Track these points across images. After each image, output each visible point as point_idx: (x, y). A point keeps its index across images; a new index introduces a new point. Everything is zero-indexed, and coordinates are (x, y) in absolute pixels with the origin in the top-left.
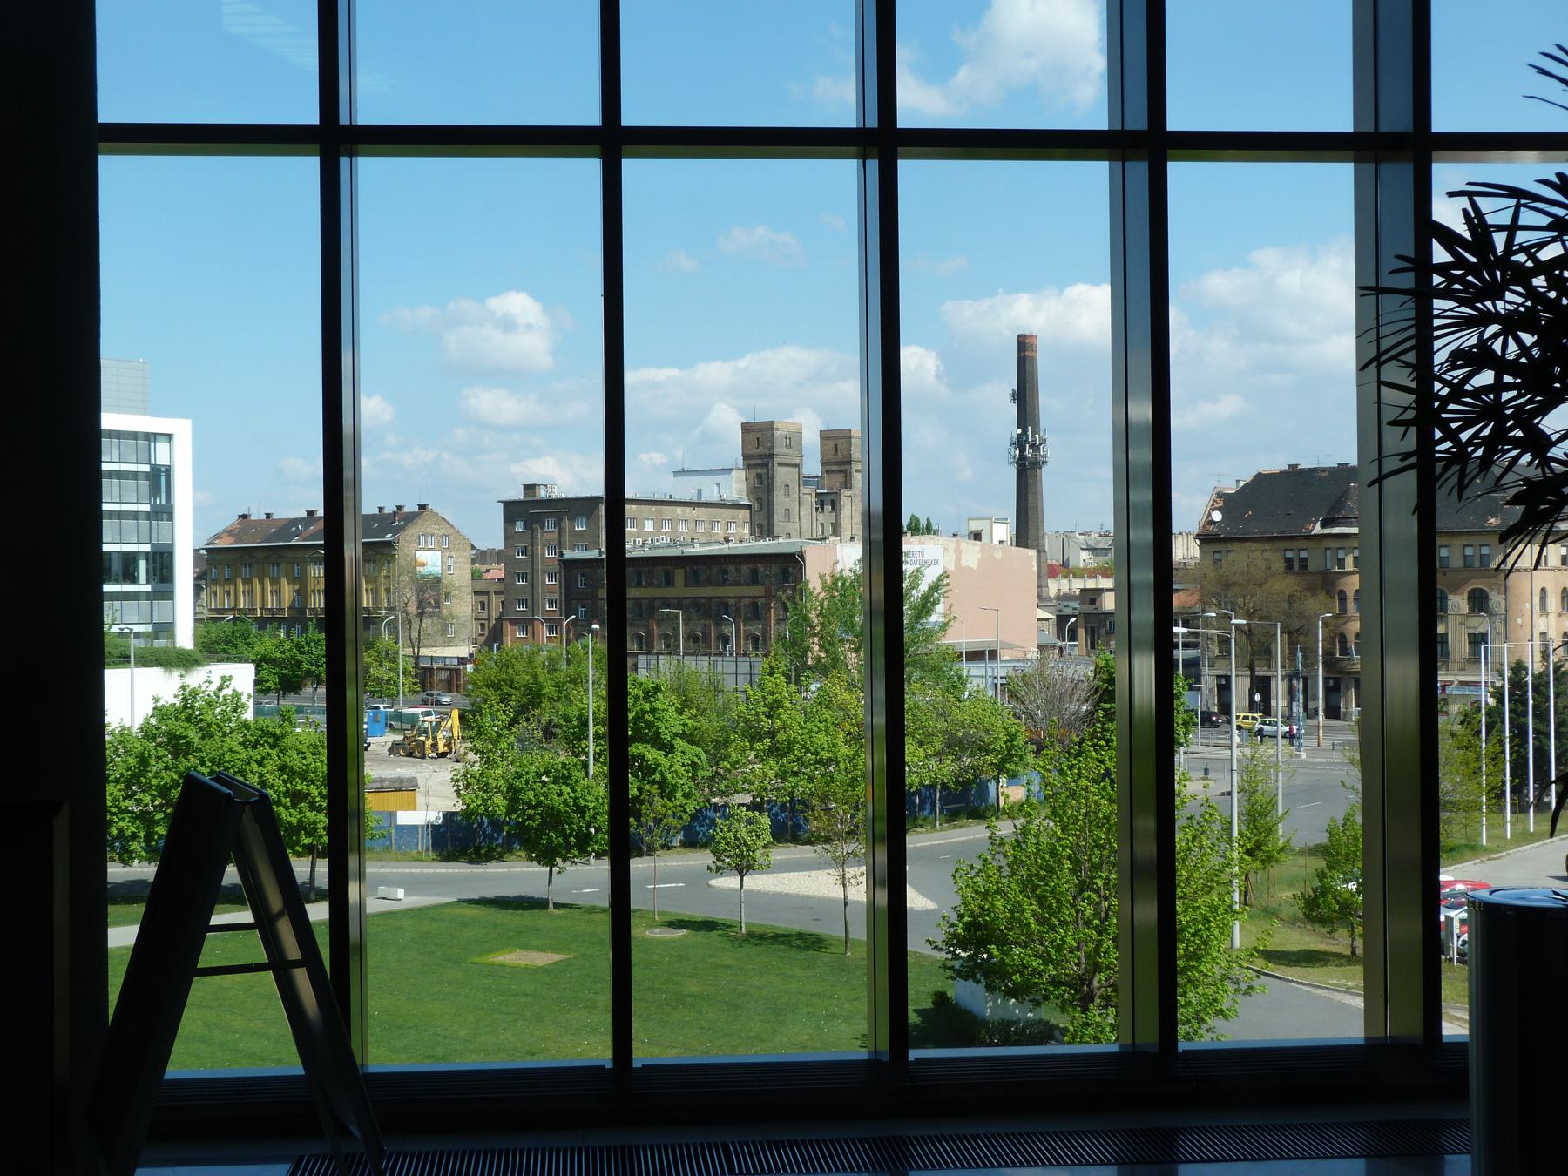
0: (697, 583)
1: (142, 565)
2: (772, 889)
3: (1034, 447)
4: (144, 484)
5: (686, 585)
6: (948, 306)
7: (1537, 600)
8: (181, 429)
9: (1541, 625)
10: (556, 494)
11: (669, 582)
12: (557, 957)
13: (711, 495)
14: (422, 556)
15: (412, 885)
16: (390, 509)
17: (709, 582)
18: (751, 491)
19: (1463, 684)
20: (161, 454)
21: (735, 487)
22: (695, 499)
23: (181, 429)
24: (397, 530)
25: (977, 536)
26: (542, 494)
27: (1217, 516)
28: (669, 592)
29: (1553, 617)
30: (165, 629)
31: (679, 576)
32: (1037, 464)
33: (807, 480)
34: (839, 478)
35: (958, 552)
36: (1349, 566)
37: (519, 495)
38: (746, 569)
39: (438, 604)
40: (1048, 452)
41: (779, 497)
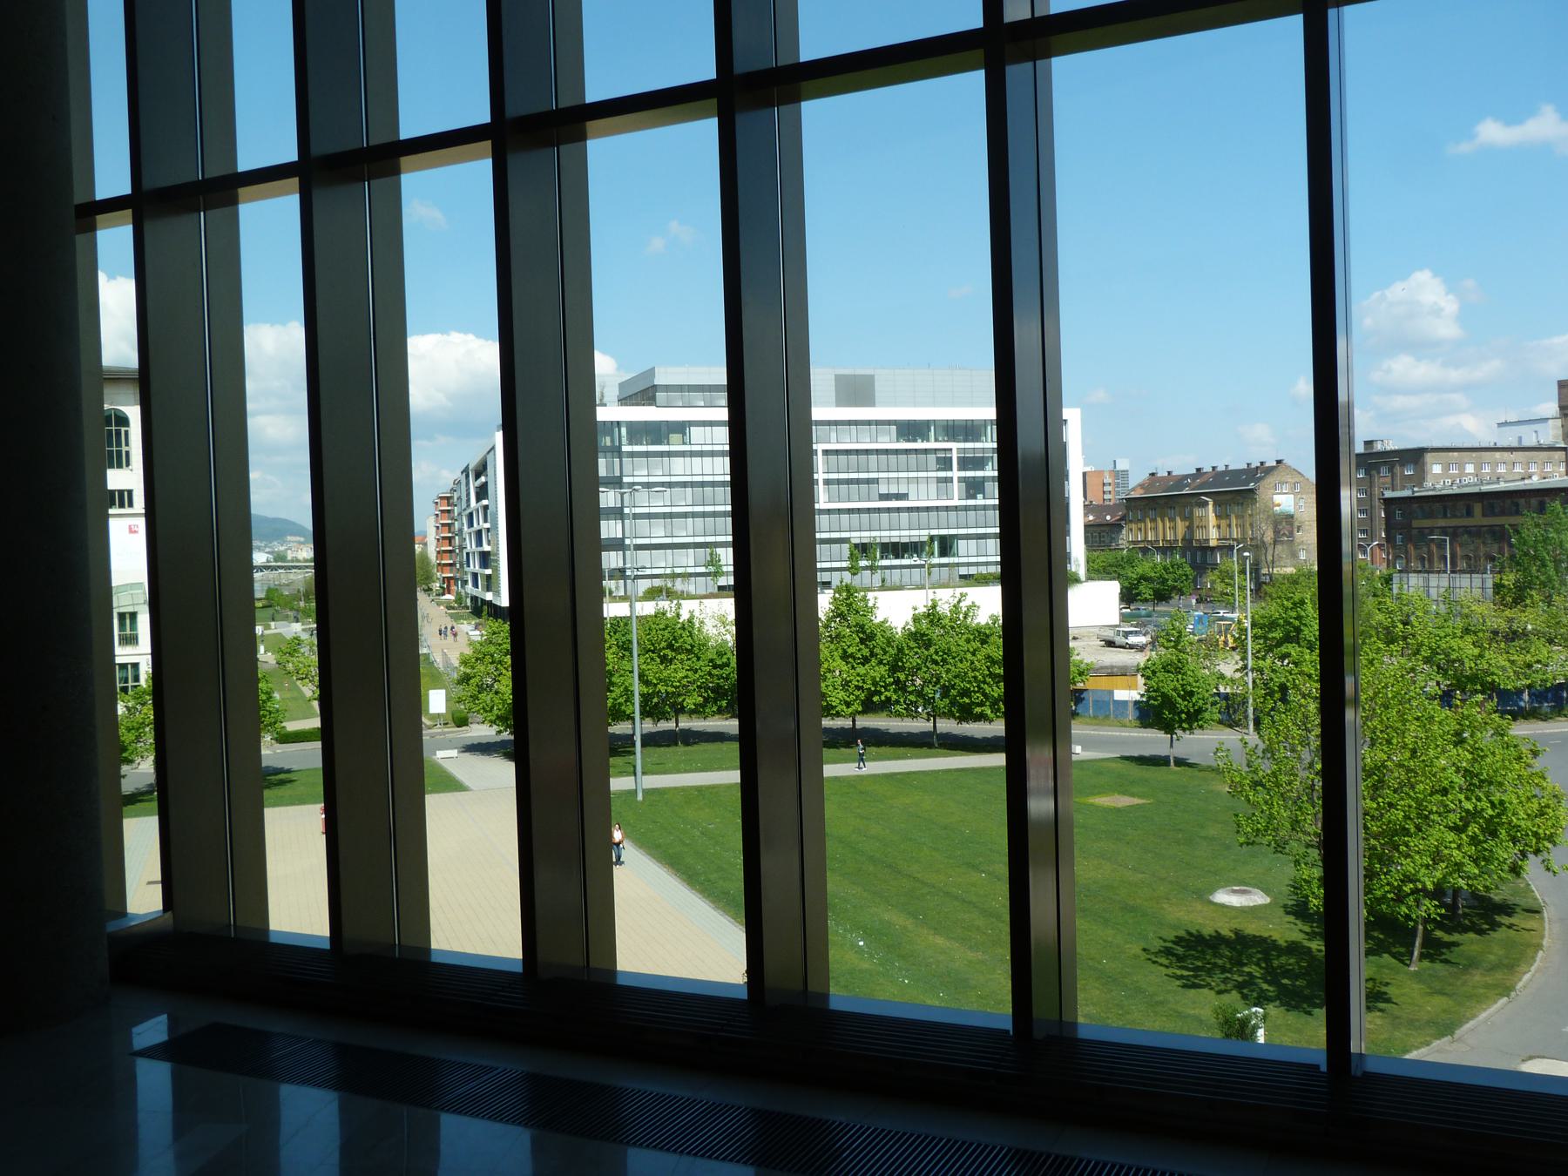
0: (1494, 514)
2: (724, 773)
5: (1484, 515)
10: (1391, 446)
12: (1137, 801)
13: (1530, 441)
14: (1277, 499)
16: (1255, 464)
17: (1503, 513)
22: (1515, 444)
26: (1379, 447)
38: (1534, 502)
39: (1291, 534)
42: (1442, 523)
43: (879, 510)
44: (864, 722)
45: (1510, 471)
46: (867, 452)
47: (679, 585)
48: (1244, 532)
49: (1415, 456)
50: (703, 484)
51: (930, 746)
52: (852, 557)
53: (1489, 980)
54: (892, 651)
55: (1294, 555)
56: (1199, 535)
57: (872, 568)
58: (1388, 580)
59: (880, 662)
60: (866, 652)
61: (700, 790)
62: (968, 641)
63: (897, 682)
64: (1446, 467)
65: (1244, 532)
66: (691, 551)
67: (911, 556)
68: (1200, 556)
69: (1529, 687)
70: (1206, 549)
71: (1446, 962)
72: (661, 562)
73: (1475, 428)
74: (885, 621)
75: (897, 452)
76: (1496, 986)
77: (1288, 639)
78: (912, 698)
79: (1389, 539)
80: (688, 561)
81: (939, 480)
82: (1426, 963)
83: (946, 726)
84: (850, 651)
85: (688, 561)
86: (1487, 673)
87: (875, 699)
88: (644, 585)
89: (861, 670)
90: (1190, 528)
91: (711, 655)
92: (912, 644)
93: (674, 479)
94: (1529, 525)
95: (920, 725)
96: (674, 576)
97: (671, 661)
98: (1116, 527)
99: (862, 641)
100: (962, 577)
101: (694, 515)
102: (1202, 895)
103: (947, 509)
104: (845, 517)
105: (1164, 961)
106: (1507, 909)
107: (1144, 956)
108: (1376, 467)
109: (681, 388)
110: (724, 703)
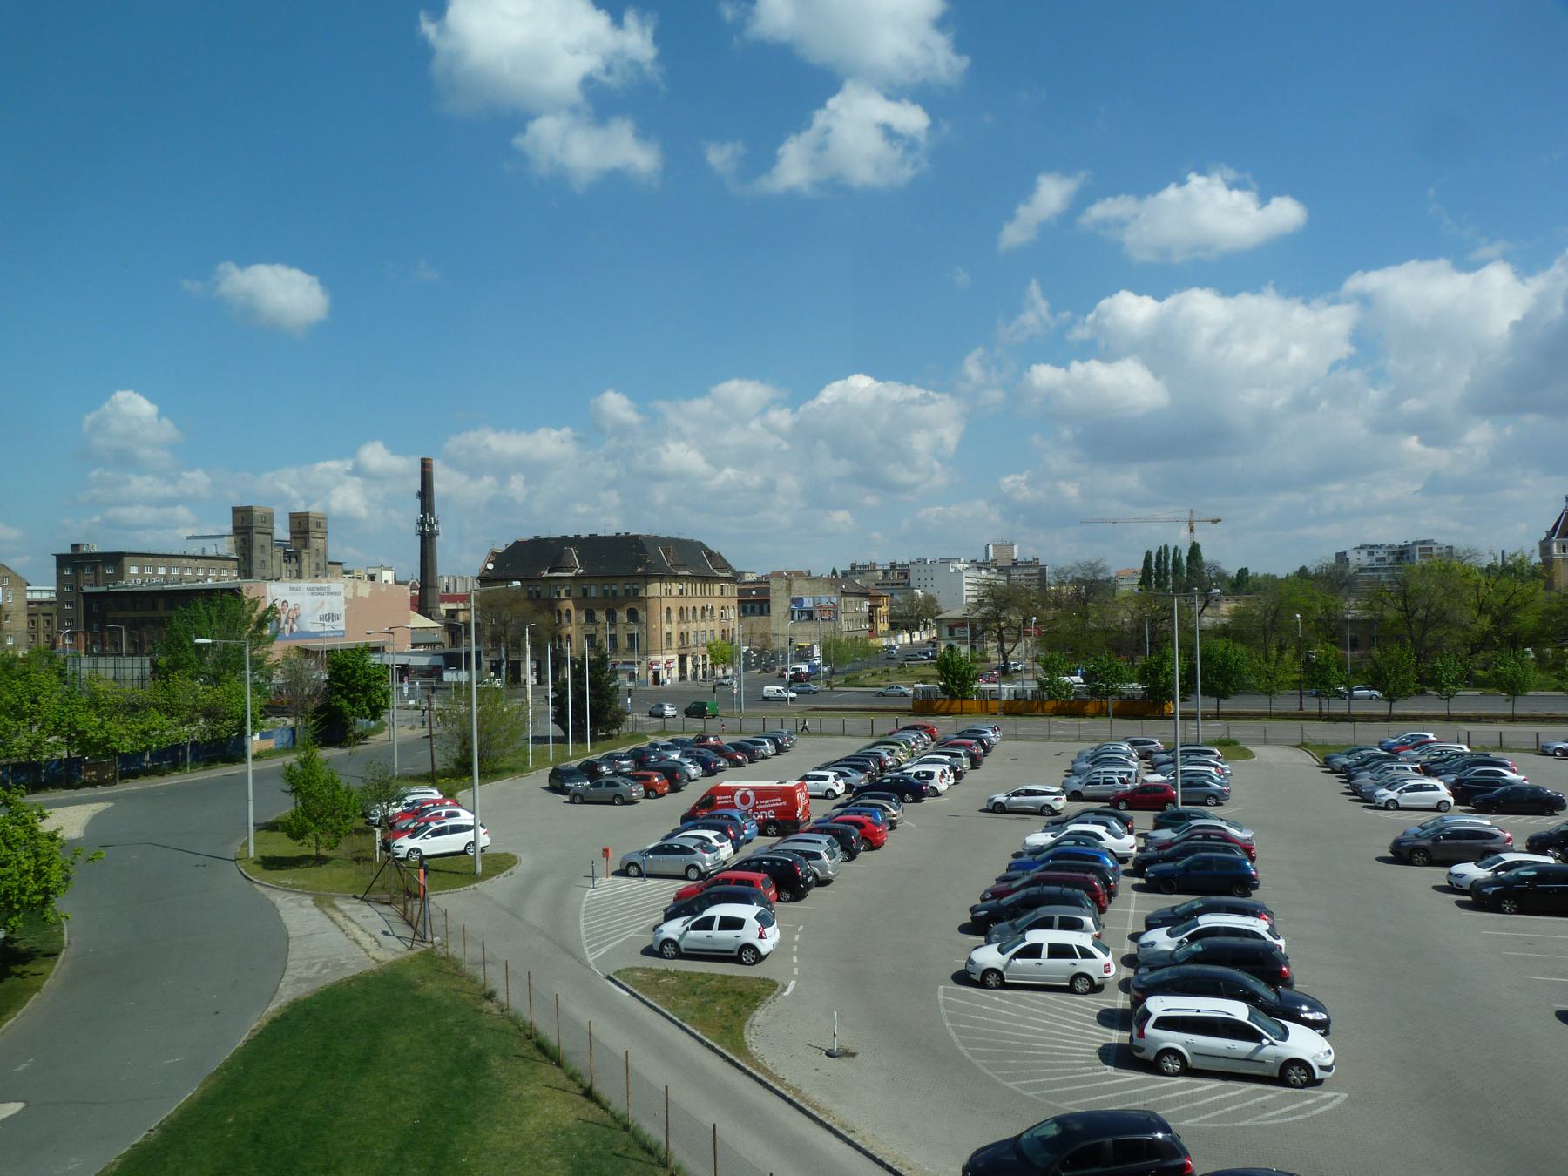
9: (667, 628)
10: (96, 549)
11: (154, 607)
13: (211, 551)
19: (625, 663)
21: (227, 547)
25: (372, 578)
27: (490, 566)
28: (151, 614)
29: (674, 624)
31: (161, 603)
32: (433, 535)
33: (281, 544)
34: (300, 543)
35: (355, 587)
36: (563, 595)
37: (67, 550)
40: (439, 528)
41: (257, 553)
42: (131, 614)
45: (194, 574)
64: (142, 570)
69: (148, 748)
73: (175, 540)
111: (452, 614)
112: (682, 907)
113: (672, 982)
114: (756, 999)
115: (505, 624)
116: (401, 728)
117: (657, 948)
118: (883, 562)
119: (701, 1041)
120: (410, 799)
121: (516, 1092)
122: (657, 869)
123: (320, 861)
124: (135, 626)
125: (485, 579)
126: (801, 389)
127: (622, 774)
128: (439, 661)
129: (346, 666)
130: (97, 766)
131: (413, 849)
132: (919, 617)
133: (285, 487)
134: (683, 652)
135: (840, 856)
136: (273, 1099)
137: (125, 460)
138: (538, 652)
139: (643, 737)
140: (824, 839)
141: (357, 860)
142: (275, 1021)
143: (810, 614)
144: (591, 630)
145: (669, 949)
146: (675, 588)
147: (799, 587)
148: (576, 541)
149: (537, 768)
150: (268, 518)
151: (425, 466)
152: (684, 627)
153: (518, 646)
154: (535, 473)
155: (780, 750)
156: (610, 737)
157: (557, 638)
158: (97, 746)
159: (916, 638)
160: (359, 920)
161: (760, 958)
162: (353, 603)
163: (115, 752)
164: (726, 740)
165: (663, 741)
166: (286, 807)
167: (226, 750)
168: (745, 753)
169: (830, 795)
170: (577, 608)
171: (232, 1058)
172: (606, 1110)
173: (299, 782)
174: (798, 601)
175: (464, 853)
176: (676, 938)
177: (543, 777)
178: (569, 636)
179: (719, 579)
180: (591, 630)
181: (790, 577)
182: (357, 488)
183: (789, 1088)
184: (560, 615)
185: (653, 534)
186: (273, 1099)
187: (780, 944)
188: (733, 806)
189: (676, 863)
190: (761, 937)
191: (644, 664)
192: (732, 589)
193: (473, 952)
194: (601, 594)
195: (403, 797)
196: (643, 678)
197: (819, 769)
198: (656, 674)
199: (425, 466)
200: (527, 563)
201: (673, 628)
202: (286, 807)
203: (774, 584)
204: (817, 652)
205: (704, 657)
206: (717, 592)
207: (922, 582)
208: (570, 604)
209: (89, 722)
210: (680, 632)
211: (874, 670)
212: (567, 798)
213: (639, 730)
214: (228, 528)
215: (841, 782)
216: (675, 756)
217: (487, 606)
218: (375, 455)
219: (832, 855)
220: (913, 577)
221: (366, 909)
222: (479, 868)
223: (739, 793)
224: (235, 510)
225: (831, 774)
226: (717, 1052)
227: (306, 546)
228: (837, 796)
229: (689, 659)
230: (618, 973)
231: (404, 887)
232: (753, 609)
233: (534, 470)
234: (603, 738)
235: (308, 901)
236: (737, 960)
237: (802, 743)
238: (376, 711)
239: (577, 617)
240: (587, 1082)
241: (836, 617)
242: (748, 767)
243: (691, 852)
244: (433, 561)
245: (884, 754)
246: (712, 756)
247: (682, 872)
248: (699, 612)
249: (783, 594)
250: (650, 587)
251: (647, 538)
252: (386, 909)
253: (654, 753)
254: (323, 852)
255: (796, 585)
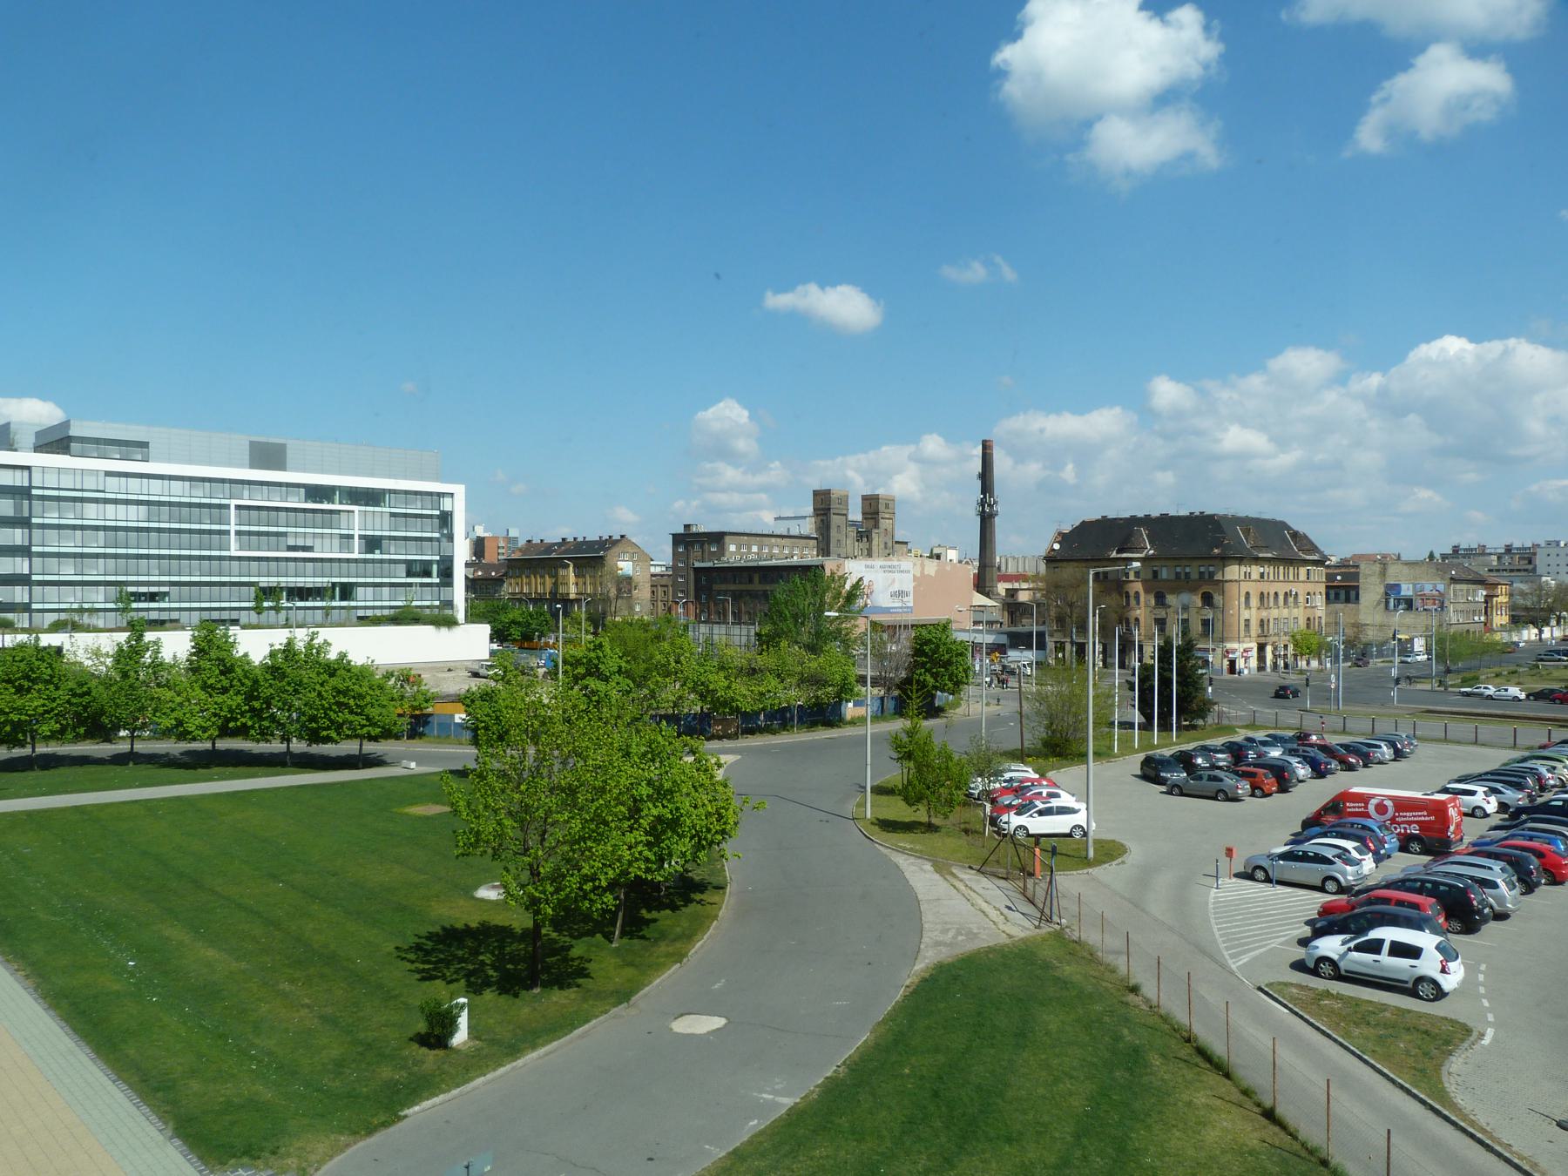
1: (435, 567)
3: (990, 506)
4: (436, 521)
6: (701, 415)
7: (1243, 599)
8: (459, 490)
9: (1245, 614)
10: (702, 530)
14: (620, 564)
15: (420, 760)
18: (818, 529)
20: (447, 505)
21: (808, 527)
23: (459, 490)
24: (606, 550)
26: (694, 530)
27: (1057, 546)
29: (1254, 610)
30: (449, 604)
31: (756, 578)
32: (992, 516)
33: (854, 524)
34: (872, 522)
35: (923, 565)
37: (681, 530)
40: (998, 508)
41: (833, 533)
42: (733, 587)
43: (287, 559)
44: (223, 744)
46: (277, 509)
47: (86, 619)
48: (595, 588)
49: (718, 538)
50: (116, 529)
51: (283, 764)
52: (257, 599)
53: (671, 949)
54: (248, 683)
55: (631, 608)
56: (562, 590)
57: (277, 609)
58: (686, 627)
59: (238, 693)
60: (226, 683)
61: (30, 814)
62: (319, 674)
63: (252, 710)
64: (739, 547)
65: (595, 588)
66: (102, 588)
67: (314, 600)
68: (560, 603)
70: (567, 602)
71: (643, 937)
72: (71, 598)
73: (766, 520)
74: (246, 655)
75: (305, 510)
76: (672, 955)
77: (589, 673)
78: (266, 723)
79: (697, 597)
80: (98, 598)
81: (342, 536)
82: (625, 940)
83: (298, 746)
84: (212, 681)
85: (98, 598)
86: (733, 699)
87: (231, 725)
88: (50, 618)
89: (220, 699)
90: (555, 584)
91: (71, 685)
92: (268, 677)
93: (86, 523)
94: (780, 590)
95: (276, 746)
96: (81, 611)
97: (29, 690)
98: (499, 581)
99: (222, 673)
100: (360, 618)
101: (105, 556)
102: (468, 891)
103: (348, 561)
104: (254, 564)
105: (412, 956)
106: (701, 887)
107: (395, 953)
108: (692, 544)
109: (97, 441)
110: (82, 730)
111: (1012, 593)
112: (1326, 924)
113: (1337, 1005)
114: (1447, 1042)
115: (1071, 605)
116: (978, 707)
117: (1311, 965)
118: (1496, 543)
119: (1393, 1081)
120: (1007, 776)
121: (1185, 1097)
122: (1287, 877)
123: (930, 828)
124: (737, 597)
125: (1051, 559)
126: (1388, 355)
127: (1220, 768)
128: (1004, 640)
129: (928, 642)
130: (723, 721)
131: (1020, 827)
132: (1551, 610)
133: (850, 473)
134: (1262, 640)
135: (1519, 888)
136: (941, 1058)
137: (721, 450)
138: (1106, 632)
139: (1230, 730)
140: (1497, 866)
141: (966, 831)
142: (924, 980)
143: (1409, 604)
144: (1161, 613)
145: (1326, 969)
146: (1256, 571)
147: (1394, 574)
148: (1147, 521)
149: (1123, 755)
150: (844, 500)
151: (986, 447)
152: (1264, 614)
153: (1083, 628)
154: (1096, 453)
155: (1398, 755)
156: (1194, 727)
157: (1124, 620)
158: (725, 704)
159: (1547, 633)
160: (981, 891)
161: (1439, 994)
162: (920, 581)
163: (738, 709)
164: (1333, 740)
165: (1260, 735)
166: (895, 774)
167: (823, 714)
168: (1358, 756)
169: (1478, 813)
170: (1147, 591)
171: (894, 1009)
172: (1295, 1138)
173: (907, 751)
174: (1395, 588)
175: (1069, 835)
176: (1335, 957)
177: (1135, 762)
178: (1137, 620)
179: (1305, 562)
180: (1161, 613)
181: (1384, 562)
182: (917, 473)
183: (1522, 1158)
184: (1136, 594)
185: (1230, 512)
186: (941, 1058)
187: (1464, 982)
188: (1367, 815)
189: (1314, 872)
190: (1443, 971)
191: (1219, 651)
192: (1319, 573)
193: (1114, 942)
194: (1173, 577)
195: (998, 774)
196: (1217, 666)
197: (1459, 781)
198: (1232, 663)
199: (986, 447)
200: (1093, 544)
201: (1253, 614)
202: (895, 774)
203: (1364, 568)
204: (1419, 644)
205: (1286, 647)
206: (1303, 577)
207: (1553, 569)
208: (1138, 587)
209: (718, 682)
210: (1258, 620)
211: (1497, 669)
212: (1163, 788)
213: (1225, 722)
214: (810, 510)
215: (1493, 799)
216: (1275, 753)
217: (1054, 587)
218: (933, 445)
219: (1511, 886)
220: (1540, 561)
221: (985, 882)
222: (1091, 854)
223: (1374, 802)
224: (816, 493)
225: (1480, 790)
226: (1415, 1096)
227: (876, 526)
228: (1487, 815)
229: (1269, 649)
230: (1270, 985)
231: (1025, 862)
232: (1337, 595)
233: (1084, 453)
234: (1187, 728)
235: (928, 866)
236: (1413, 993)
237: (1424, 751)
238: (957, 685)
239: (1148, 600)
240: (1268, 1103)
241: (1442, 607)
242: (1362, 772)
243: (1330, 862)
244: (992, 541)
245: (1543, 770)
246: (1322, 756)
247: (1319, 884)
248: (1281, 598)
249: (1375, 579)
250: (1227, 569)
251: (1225, 517)
252: (1002, 883)
253: (1251, 748)
254: (934, 821)
255: (1393, 570)
